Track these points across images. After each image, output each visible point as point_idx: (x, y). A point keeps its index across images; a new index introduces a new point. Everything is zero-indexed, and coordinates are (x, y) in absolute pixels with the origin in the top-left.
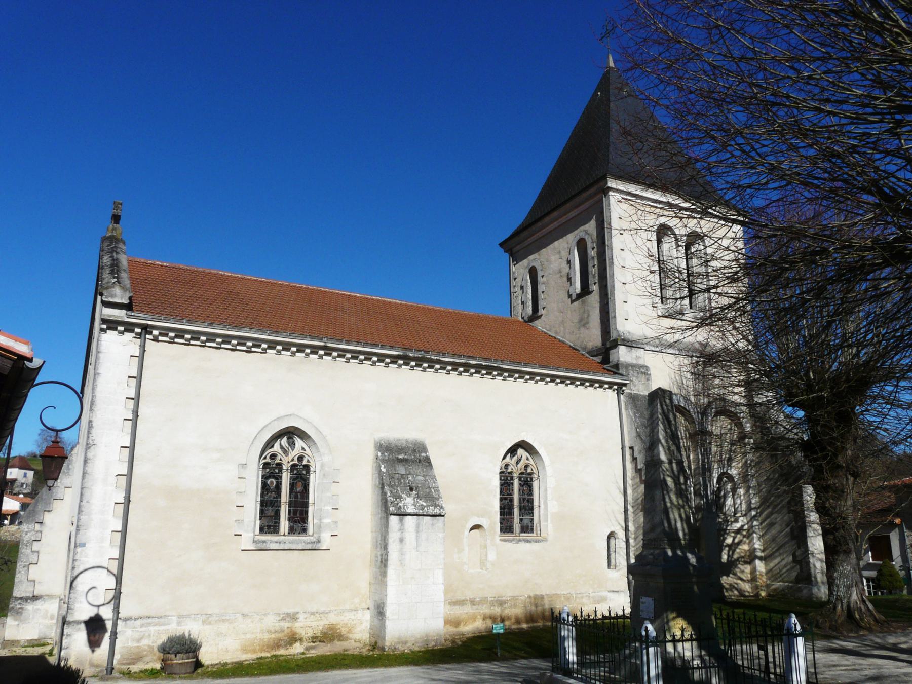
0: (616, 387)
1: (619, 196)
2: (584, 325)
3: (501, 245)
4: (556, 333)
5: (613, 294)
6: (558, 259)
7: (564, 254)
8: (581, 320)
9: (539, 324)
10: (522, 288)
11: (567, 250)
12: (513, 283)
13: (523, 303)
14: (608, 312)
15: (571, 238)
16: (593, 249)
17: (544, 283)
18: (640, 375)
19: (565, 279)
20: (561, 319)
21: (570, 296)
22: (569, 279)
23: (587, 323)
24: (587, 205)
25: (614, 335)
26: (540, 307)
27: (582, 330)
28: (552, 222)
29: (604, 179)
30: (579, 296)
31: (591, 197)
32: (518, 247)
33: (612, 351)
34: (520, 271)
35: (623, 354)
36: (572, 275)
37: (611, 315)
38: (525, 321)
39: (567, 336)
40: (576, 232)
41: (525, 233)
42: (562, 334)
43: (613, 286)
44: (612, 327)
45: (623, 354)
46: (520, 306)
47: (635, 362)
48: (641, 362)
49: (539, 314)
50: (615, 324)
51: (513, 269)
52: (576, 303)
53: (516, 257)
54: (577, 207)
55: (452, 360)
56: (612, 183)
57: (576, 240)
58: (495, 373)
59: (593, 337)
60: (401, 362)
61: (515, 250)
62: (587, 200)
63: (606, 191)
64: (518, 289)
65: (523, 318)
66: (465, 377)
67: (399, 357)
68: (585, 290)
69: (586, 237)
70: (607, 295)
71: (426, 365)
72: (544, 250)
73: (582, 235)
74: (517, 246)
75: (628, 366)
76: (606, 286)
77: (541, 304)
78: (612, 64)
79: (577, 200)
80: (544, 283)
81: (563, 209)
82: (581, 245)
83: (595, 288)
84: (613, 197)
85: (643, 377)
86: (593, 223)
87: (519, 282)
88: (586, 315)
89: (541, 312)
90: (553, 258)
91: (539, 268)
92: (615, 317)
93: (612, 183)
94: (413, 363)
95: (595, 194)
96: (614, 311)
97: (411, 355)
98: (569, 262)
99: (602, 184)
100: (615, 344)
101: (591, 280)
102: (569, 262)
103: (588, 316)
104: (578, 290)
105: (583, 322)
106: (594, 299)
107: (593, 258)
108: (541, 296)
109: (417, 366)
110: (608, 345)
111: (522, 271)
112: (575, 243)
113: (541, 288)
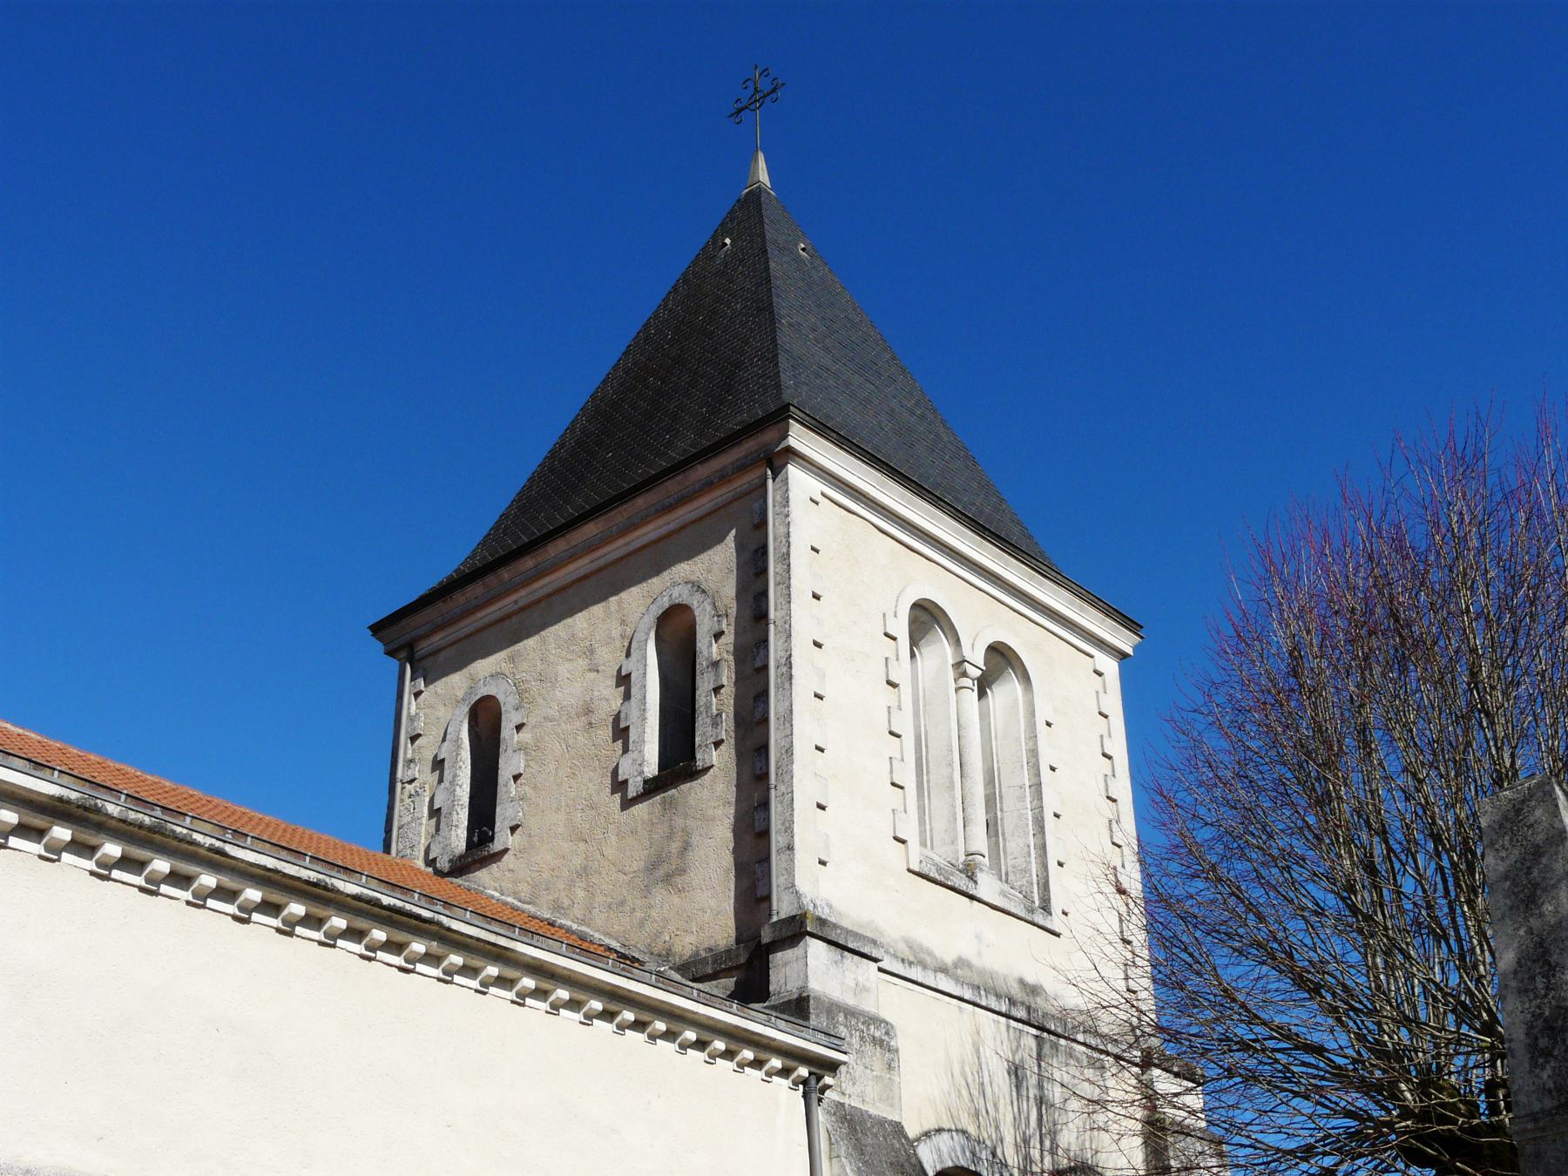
0: (803, 1071)
1: (815, 486)
2: (667, 879)
3: (377, 629)
4: (557, 907)
5: (787, 774)
6: (578, 674)
7: (610, 658)
8: (652, 866)
9: (486, 880)
10: (438, 764)
11: (620, 644)
12: (406, 750)
13: (435, 813)
14: (765, 834)
15: (638, 604)
16: (718, 635)
17: (522, 748)
18: (868, 1048)
19: (606, 733)
20: (578, 861)
21: (619, 786)
22: (621, 733)
23: (682, 871)
24: (705, 503)
25: (782, 907)
26: (502, 825)
27: (659, 894)
28: (573, 556)
29: (779, 417)
30: (653, 787)
31: (723, 477)
32: (437, 639)
33: (778, 958)
34: (437, 711)
35: (815, 969)
36: (632, 720)
37: (777, 840)
38: (438, 873)
39: (599, 918)
40: (656, 583)
41: (475, 591)
42: (578, 912)
43: (789, 751)
44: (777, 880)
45: (815, 969)
46: (426, 825)
47: (850, 1000)
48: (868, 1005)
49: (497, 846)
50: (790, 871)
51: (410, 706)
52: (640, 809)
53: (429, 667)
54: (671, 508)
55: (270, 862)
56: (799, 438)
57: (657, 610)
58: (418, 947)
59: (707, 914)
60: (62, 833)
61: (424, 647)
62: (708, 485)
63: (779, 459)
64: (424, 774)
65: (430, 862)
66: (304, 948)
67: (58, 810)
68: (680, 762)
69: (695, 602)
70: (765, 776)
71: (162, 865)
72: (531, 642)
73: (681, 594)
74: (420, 636)
75: (833, 1008)
76: (763, 749)
77: (505, 813)
78: (763, 176)
79: (673, 486)
80: (522, 748)
81: (619, 515)
82: (676, 633)
83: (718, 758)
84: (798, 479)
85: (876, 1057)
86: (716, 567)
87: (428, 747)
88: (675, 847)
89: (502, 838)
90: (563, 670)
91: (507, 701)
92: (790, 848)
93: (799, 438)
94: (113, 849)
95: (742, 468)
96: (789, 830)
97: (112, 809)
98: (623, 680)
99: (768, 436)
100: (796, 930)
101: (703, 732)
102: (623, 680)
103: (686, 847)
104: (652, 769)
105: (665, 869)
106: (713, 796)
107: (715, 665)
108: (507, 789)
109: (125, 863)
110: (766, 936)
111: (443, 713)
112: (650, 620)
113: (509, 764)
